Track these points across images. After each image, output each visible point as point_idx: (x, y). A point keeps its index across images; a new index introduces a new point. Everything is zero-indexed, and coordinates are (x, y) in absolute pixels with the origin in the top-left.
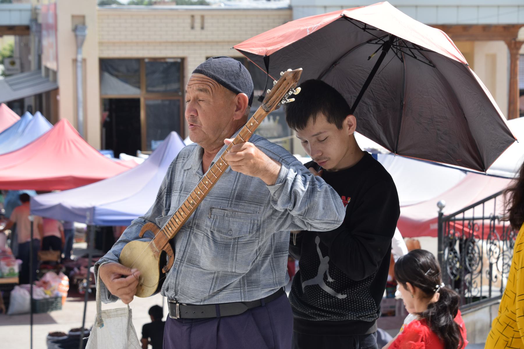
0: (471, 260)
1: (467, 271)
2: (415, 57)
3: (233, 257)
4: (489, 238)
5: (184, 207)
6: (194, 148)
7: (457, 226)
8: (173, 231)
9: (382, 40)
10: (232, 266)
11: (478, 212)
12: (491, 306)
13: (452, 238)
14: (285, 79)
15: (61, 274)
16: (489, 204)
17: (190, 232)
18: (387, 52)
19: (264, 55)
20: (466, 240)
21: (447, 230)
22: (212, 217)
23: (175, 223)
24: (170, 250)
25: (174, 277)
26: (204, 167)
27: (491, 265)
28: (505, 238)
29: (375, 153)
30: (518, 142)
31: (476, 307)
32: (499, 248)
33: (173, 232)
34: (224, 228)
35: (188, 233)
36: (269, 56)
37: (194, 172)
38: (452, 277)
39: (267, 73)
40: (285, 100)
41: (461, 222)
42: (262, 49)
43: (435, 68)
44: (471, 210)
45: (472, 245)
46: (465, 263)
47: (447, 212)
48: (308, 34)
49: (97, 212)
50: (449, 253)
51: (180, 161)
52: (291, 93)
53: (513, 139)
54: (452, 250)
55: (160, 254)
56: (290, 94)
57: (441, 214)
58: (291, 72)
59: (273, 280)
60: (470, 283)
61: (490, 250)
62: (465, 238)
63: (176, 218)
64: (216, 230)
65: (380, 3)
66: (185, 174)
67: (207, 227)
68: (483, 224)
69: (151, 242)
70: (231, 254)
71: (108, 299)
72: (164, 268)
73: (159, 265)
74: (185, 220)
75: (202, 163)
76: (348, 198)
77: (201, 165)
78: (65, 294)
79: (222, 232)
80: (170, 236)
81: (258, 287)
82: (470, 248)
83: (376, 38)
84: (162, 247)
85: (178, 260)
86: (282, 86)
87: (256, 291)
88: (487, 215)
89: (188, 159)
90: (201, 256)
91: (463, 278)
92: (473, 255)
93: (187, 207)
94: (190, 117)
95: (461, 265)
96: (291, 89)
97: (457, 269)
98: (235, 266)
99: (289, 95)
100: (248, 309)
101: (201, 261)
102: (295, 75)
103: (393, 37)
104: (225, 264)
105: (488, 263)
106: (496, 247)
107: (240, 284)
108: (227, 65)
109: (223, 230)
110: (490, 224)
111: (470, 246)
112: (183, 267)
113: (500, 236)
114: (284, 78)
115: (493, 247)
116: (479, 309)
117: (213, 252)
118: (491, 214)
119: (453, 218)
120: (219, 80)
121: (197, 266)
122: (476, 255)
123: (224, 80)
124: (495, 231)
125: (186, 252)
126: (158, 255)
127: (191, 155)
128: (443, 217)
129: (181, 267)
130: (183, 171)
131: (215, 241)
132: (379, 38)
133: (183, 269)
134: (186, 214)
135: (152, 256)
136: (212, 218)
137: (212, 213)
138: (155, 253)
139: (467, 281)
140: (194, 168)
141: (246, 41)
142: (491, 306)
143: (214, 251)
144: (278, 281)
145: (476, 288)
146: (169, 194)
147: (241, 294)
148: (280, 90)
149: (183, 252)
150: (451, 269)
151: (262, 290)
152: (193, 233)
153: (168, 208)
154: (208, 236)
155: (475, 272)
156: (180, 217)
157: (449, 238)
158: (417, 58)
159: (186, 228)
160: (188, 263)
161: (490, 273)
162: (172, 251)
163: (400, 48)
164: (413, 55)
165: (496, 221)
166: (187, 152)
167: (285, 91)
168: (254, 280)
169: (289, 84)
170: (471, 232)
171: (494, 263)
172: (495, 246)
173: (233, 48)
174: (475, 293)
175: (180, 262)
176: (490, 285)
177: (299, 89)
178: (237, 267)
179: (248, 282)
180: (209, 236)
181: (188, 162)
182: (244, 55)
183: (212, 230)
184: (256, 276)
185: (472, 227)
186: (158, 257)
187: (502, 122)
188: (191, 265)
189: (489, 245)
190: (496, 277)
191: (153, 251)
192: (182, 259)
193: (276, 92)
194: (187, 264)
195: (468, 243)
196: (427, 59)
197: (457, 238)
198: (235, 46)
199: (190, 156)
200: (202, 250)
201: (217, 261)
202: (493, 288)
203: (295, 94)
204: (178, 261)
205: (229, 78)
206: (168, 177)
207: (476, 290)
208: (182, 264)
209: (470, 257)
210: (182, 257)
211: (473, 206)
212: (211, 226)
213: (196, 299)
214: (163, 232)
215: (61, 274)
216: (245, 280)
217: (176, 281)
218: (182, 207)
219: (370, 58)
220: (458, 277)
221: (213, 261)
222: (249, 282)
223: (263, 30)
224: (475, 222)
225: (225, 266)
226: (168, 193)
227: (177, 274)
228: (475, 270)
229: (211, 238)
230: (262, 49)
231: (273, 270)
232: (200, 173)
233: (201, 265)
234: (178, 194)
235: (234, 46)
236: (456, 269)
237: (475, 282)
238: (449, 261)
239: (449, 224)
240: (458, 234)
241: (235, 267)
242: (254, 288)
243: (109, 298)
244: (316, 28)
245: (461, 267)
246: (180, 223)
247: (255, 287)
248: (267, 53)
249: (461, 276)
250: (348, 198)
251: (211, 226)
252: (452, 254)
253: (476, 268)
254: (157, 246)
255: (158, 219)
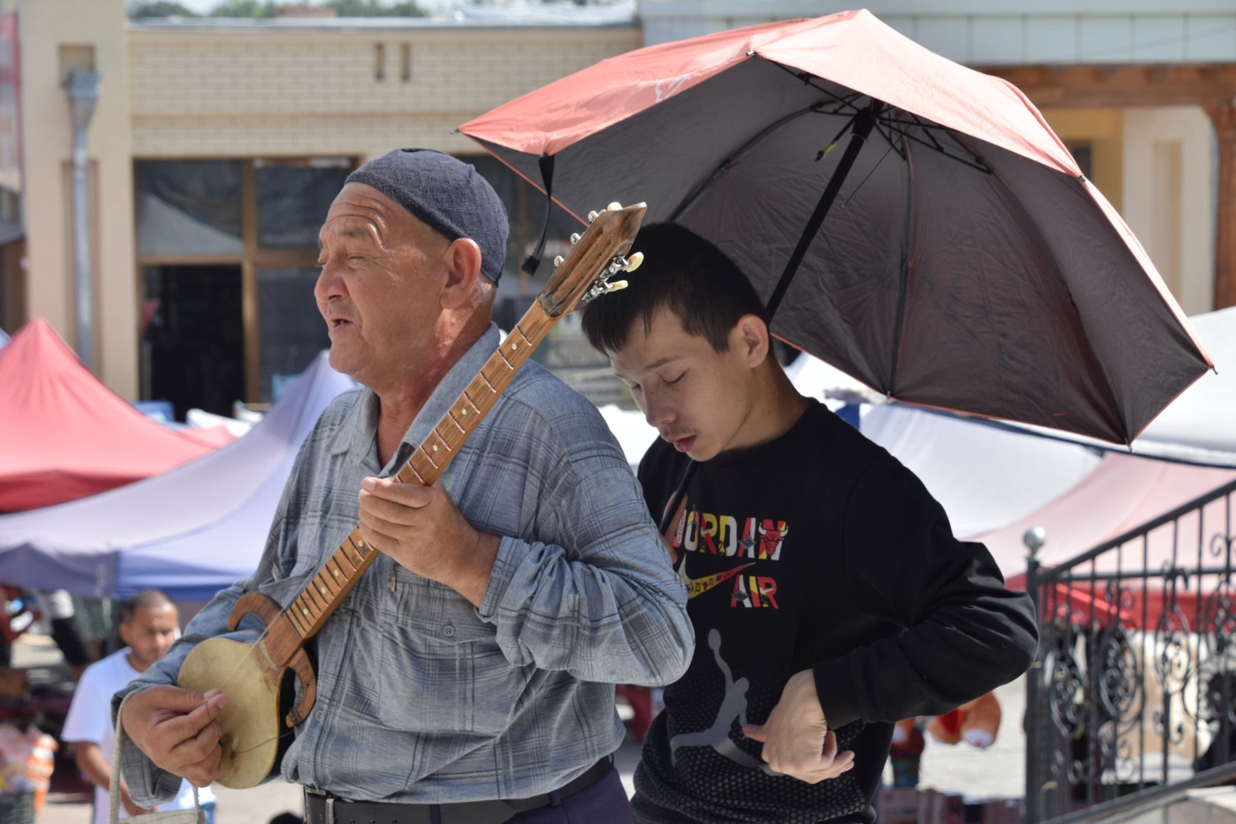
0: (1113, 685)
1: (1104, 716)
2: (940, 149)
3: (465, 694)
4: (1160, 626)
5: (341, 557)
6: (358, 398)
7: (1076, 595)
8: (312, 618)
9: (849, 104)
10: (464, 716)
11: (1131, 557)
12: (1167, 806)
13: (1064, 627)
14: (600, 232)
15: (33, 731)
16: (1160, 538)
17: (351, 623)
18: (866, 139)
19: (540, 153)
20: (1101, 632)
21: (1050, 605)
22: (398, 587)
23: (317, 598)
24: (307, 668)
25: (312, 743)
26: (382, 449)
27: (1167, 698)
28: (1202, 627)
29: (852, 401)
30: (1216, 373)
31: (1127, 810)
32: (1188, 651)
33: (313, 622)
34: (432, 618)
35: (347, 626)
36: (553, 156)
37: (357, 462)
38: (1065, 731)
39: (545, 192)
40: (602, 286)
41: (1087, 585)
42: (535, 138)
43: (992, 176)
44: (1112, 554)
45: (1115, 645)
46: (1098, 694)
47: (1050, 558)
48: (659, 100)
49: (125, 565)
50: (1056, 668)
51: (325, 433)
52: (617, 270)
53: (1204, 365)
54: (1066, 660)
55: (280, 677)
56: (612, 270)
57: (1033, 565)
58: (616, 213)
59: (585, 742)
60: (1113, 747)
61: (1165, 657)
62: (1096, 627)
63: (322, 584)
64: (409, 624)
65: (846, 13)
66: (337, 468)
67: (388, 616)
68: (1145, 590)
69: (257, 642)
70: (457, 686)
71: (151, 795)
72: (290, 714)
73: (277, 704)
74: (343, 590)
75: (377, 440)
76: (779, 522)
77: (374, 443)
78: (42, 785)
79: (426, 629)
80: (304, 631)
81: (543, 767)
82: (1112, 654)
83: (834, 99)
84: (285, 659)
85: (322, 698)
86: (591, 249)
87: (539, 778)
88: (1155, 564)
89: (343, 426)
90: (382, 694)
91: (1092, 733)
92: (1121, 671)
93: (350, 556)
94: (329, 302)
95: (1087, 696)
96: (615, 259)
97: (1079, 708)
98: (470, 717)
99: (610, 273)
100: (516, 814)
101: (382, 706)
102: (627, 217)
103: (877, 105)
104: (444, 712)
105: (1159, 691)
106: (1178, 650)
107: (496, 762)
108: (435, 166)
109: (428, 625)
110: (1165, 589)
111: (1110, 647)
112: (337, 718)
113: (1188, 620)
114: (597, 229)
115: (1171, 651)
116: (1136, 815)
117: (411, 682)
118: (1166, 562)
119: (1065, 575)
120: (406, 199)
121: (371, 718)
122: (1128, 673)
123: (419, 200)
124: (1178, 608)
125: (343, 679)
126: (276, 679)
127: (351, 415)
128: (1040, 572)
129: (331, 717)
130: (329, 457)
131: (412, 652)
132: (842, 100)
133: (336, 724)
134: (347, 575)
135: (260, 681)
136: (398, 592)
137: (399, 580)
138: (266, 675)
139: (1104, 741)
140: (355, 451)
141: (491, 112)
142: (1167, 806)
143: (412, 680)
144: (598, 745)
145: (1128, 758)
146: (291, 520)
147: (498, 786)
148: (586, 260)
149: (335, 677)
150: (1062, 708)
151: (555, 773)
152: (358, 626)
153: (290, 556)
154: (393, 639)
155: (1127, 717)
156: (331, 583)
157: (1057, 629)
158: (946, 150)
159: (341, 613)
160: (348, 709)
161: (1165, 719)
162: (311, 670)
163: (898, 125)
164: (932, 143)
165: (1180, 583)
166: (341, 409)
167: (601, 263)
168: (533, 749)
169: (610, 243)
170: (1114, 610)
171: (1175, 692)
172: (1178, 647)
173: (458, 131)
174: (1125, 772)
175: (330, 705)
176: (1166, 752)
177: (639, 257)
178: (476, 719)
179: (516, 756)
180: (396, 640)
181: (342, 434)
182: (489, 149)
183: (400, 625)
184: (536, 737)
185: (1117, 597)
186: (276, 685)
187: (1173, 321)
188: (356, 715)
189: (1161, 647)
190: (1180, 730)
191: (262, 667)
192: (332, 697)
193: (577, 263)
194: (346, 711)
195: (1104, 641)
196: (970, 153)
197: (1076, 628)
198: (465, 125)
199: (348, 416)
200: (382, 676)
201: (423, 706)
202: (1173, 759)
203: (628, 271)
204: (324, 702)
205: (433, 195)
206: (294, 477)
207: (1129, 765)
208: (335, 711)
209: (1112, 677)
210: (334, 692)
211: (1117, 543)
212: (398, 613)
213: (374, 794)
214: (288, 620)
215: (33, 731)
216: (507, 750)
217: (315, 755)
218: (335, 557)
219: (821, 154)
220: (1080, 730)
221: (412, 706)
222: (519, 755)
223: (538, 83)
224: (1124, 584)
225: (444, 717)
226: (291, 518)
227: (320, 736)
228: (1126, 711)
229: (401, 645)
230: (535, 138)
231: (580, 718)
232: (372, 466)
233: (381, 715)
234: (317, 520)
235: (461, 127)
236: (1075, 709)
237: (1124, 743)
238: (1056, 690)
239: (1055, 593)
240: (1078, 618)
241: (473, 719)
242: (533, 769)
243: (153, 793)
244: (678, 86)
245: (1087, 704)
246: (330, 598)
247: (536, 768)
248: (547, 147)
249: (1087, 728)
250: (779, 522)
251: (396, 615)
252: (1065, 668)
253: (1128, 706)
254: (271, 655)
255: (267, 587)
